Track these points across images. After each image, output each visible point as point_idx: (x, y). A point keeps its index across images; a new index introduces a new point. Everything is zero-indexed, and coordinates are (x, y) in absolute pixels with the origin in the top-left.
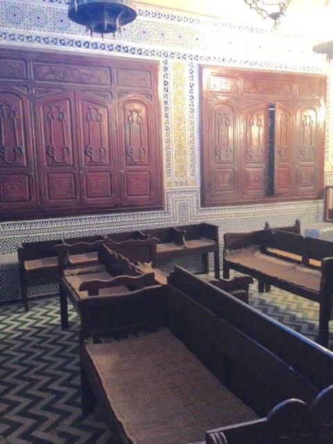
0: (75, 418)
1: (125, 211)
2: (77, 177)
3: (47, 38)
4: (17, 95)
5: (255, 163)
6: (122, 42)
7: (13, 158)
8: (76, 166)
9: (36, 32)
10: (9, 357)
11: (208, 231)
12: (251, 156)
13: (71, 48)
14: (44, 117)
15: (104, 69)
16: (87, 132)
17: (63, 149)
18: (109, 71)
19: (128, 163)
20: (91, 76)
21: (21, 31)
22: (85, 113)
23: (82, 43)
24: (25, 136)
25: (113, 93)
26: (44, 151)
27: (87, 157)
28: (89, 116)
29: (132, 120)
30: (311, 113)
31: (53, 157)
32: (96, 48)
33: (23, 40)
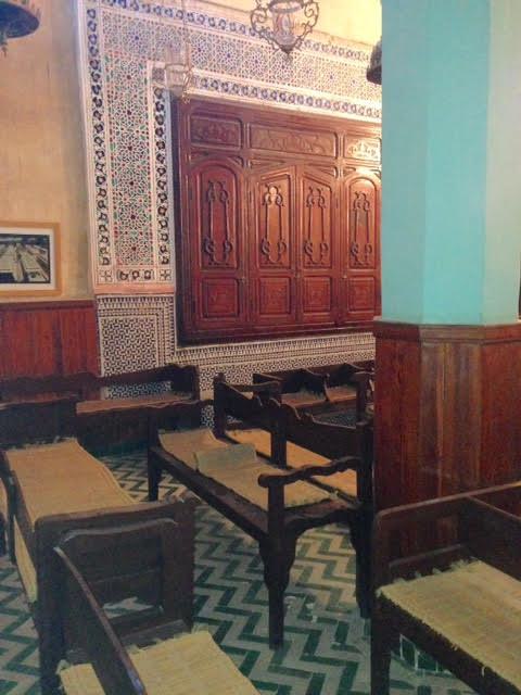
0: (11, 657)
1: (344, 332)
2: (294, 285)
3: (266, 91)
4: (230, 169)
5: (316, 267)
6: (350, 98)
7: (221, 256)
8: (293, 268)
9: (253, 82)
10: (320, 478)
11: (184, 378)
12: (309, 255)
13: (292, 105)
14: (201, 199)
15: (329, 135)
16: (263, 227)
17: (225, 242)
18: (334, 139)
19: (206, 265)
20: (315, 144)
21: (237, 80)
22: (306, 195)
23: (305, 98)
24: (237, 227)
25: (245, 159)
26: (301, 246)
27: (263, 256)
28: (267, 198)
29: (270, 200)
30: (362, 171)
31: (268, 256)
32: (320, 106)
33: (217, 88)
